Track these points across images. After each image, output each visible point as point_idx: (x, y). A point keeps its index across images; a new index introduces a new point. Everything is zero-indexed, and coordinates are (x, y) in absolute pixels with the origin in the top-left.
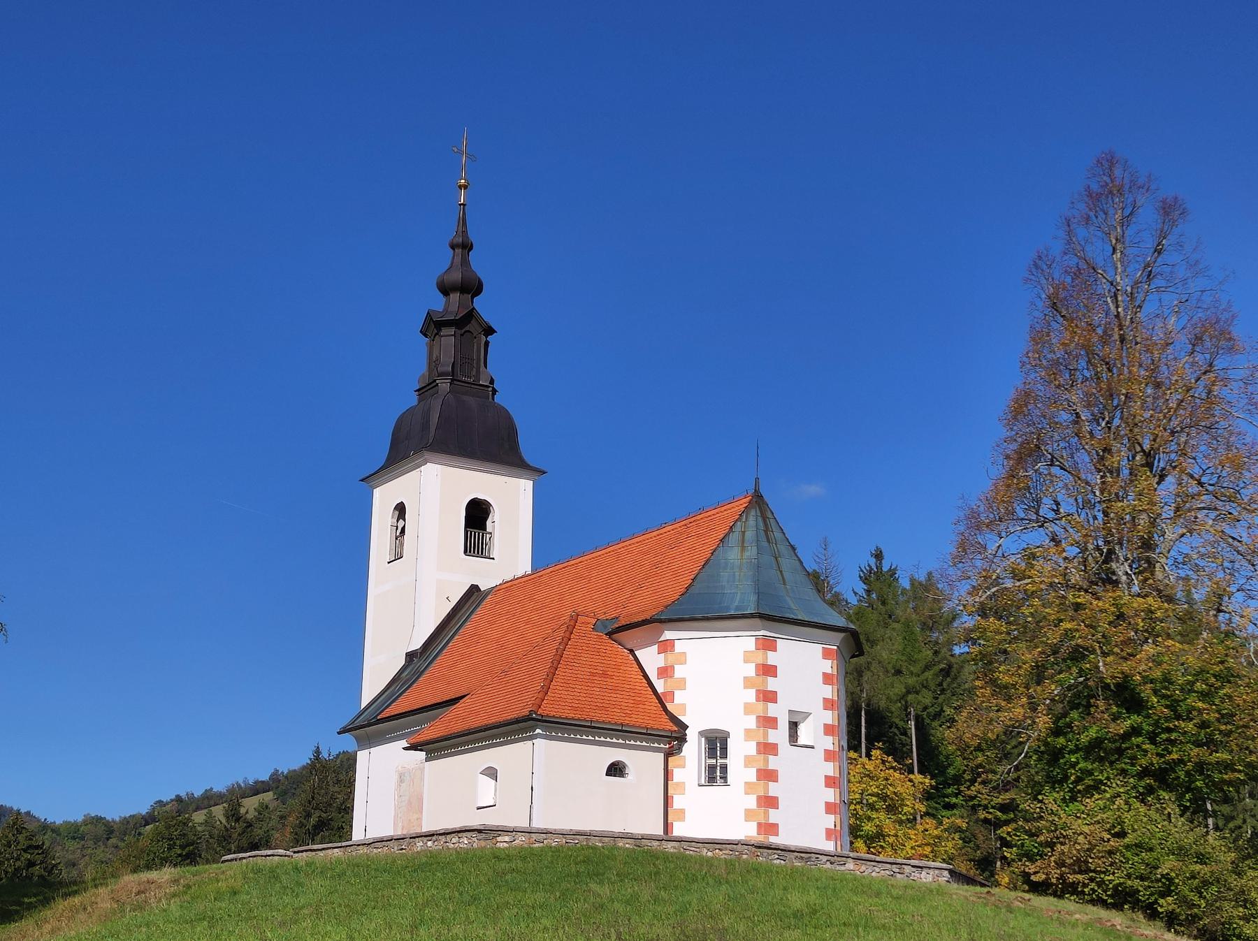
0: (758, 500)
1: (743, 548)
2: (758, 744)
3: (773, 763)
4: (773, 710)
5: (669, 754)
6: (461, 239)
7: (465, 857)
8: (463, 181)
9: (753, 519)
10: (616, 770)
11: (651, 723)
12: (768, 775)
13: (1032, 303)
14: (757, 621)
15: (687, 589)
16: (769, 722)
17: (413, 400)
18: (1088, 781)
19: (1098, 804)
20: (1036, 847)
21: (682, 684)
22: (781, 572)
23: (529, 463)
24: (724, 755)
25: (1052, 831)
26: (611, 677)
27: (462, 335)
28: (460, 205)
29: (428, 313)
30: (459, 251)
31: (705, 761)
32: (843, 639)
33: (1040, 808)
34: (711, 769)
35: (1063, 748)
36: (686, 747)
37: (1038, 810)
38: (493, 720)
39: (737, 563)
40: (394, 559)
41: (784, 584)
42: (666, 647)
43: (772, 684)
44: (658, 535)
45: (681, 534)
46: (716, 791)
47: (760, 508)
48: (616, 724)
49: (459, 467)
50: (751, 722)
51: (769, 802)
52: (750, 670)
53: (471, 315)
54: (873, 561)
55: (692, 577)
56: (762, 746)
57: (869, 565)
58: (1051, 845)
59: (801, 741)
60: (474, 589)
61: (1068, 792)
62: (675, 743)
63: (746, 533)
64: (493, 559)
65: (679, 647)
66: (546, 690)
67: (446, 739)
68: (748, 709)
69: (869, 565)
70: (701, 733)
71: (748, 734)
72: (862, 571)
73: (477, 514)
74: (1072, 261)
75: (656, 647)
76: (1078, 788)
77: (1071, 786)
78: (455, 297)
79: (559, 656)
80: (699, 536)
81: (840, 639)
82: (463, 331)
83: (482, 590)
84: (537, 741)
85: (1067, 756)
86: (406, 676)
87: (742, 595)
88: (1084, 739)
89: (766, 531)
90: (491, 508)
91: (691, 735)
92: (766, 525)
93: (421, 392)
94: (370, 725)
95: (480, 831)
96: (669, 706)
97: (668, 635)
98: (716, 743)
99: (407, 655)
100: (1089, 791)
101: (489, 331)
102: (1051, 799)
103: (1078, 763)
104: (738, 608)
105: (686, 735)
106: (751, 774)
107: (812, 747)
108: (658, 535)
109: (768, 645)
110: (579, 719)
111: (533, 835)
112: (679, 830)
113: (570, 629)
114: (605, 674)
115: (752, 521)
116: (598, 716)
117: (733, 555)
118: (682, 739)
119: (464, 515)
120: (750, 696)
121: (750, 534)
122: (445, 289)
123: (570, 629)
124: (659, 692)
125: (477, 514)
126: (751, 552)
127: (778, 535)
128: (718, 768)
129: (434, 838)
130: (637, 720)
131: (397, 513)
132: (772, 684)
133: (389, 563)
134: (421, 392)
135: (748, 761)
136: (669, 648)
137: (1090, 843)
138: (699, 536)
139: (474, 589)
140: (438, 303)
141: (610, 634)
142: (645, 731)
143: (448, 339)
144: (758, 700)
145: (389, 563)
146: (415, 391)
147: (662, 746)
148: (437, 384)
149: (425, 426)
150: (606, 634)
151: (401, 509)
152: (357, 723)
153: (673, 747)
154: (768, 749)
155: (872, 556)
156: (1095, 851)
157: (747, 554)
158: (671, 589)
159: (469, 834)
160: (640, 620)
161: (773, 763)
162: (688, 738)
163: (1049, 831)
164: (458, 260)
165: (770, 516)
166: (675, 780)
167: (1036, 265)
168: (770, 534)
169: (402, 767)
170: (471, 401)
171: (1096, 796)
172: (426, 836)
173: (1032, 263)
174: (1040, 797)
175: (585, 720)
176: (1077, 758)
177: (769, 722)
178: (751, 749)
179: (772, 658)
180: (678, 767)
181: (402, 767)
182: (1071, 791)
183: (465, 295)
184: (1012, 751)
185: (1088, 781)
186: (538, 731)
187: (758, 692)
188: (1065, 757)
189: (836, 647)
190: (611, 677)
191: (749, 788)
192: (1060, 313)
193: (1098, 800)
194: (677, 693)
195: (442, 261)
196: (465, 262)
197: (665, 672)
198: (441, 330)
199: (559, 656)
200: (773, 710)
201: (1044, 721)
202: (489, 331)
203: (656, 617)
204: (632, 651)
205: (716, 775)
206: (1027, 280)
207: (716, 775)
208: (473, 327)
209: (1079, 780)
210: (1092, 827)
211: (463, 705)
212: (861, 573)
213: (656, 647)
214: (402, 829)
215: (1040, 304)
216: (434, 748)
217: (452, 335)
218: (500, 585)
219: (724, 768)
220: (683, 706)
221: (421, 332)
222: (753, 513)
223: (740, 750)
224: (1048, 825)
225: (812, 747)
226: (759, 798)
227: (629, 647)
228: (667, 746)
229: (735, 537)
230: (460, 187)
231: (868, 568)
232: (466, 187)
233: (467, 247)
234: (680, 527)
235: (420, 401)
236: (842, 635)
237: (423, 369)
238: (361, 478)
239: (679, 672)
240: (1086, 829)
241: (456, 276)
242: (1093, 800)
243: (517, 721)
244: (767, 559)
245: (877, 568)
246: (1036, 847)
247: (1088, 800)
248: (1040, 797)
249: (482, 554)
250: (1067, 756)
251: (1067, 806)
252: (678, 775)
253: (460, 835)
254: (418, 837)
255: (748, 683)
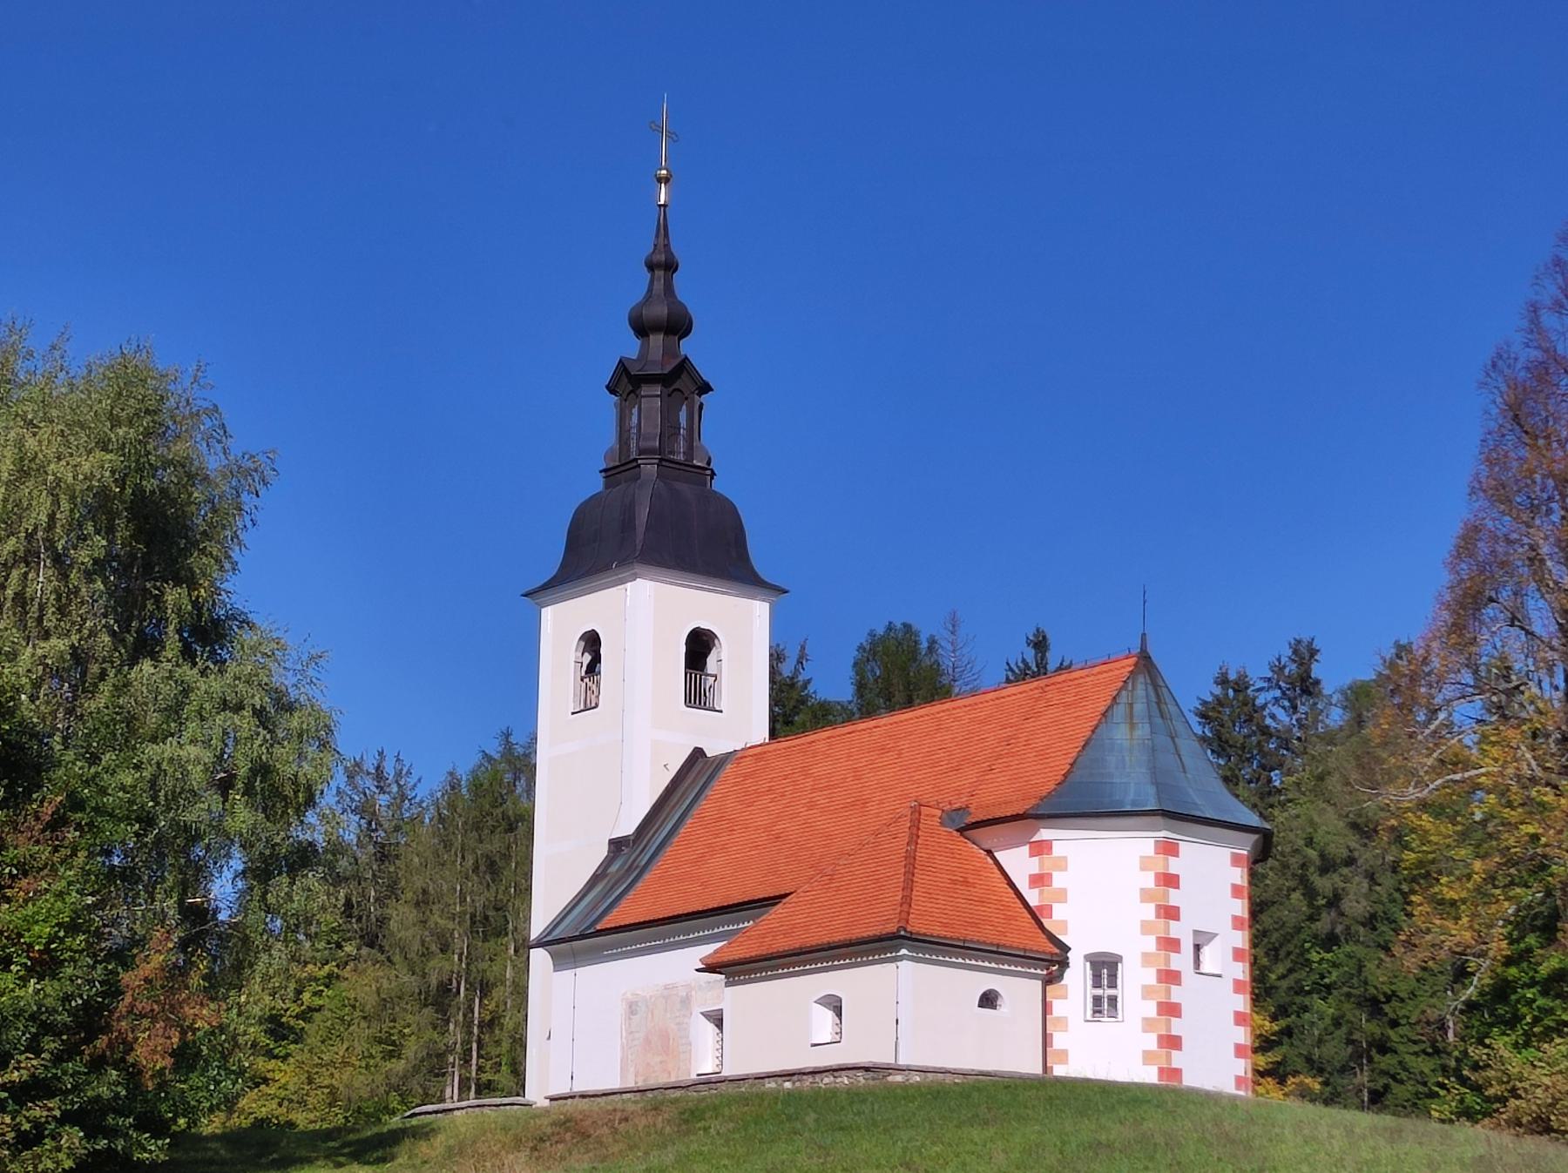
0: (1145, 662)
1: (1132, 726)
2: (1159, 971)
3: (1177, 994)
4: (1176, 929)
5: (1049, 980)
6: (663, 256)
7: (854, 1095)
8: (664, 172)
9: (1141, 688)
10: (988, 1000)
11: (1030, 945)
12: (1170, 1010)
13: (1487, 412)
14: (1159, 820)
15: (1065, 776)
16: (1171, 944)
17: (597, 484)
18: (1548, 1022)
19: (1560, 1051)
20: (1478, 1104)
21: (1062, 896)
22: (1179, 755)
23: (763, 577)
24: (1113, 985)
25: (1503, 1083)
26: (973, 885)
27: (669, 395)
28: (660, 206)
29: (620, 361)
30: (660, 273)
31: (1091, 992)
32: (1257, 841)
33: (1488, 1055)
34: (1097, 1001)
35: (1516, 981)
36: (1068, 974)
37: (1484, 1057)
38: (838, 937)
39: (1126, 744)
40: (582, 707)
41: (1185, 772)
42: (1041, 849)
43: (1174, 897)
44: (997, 699)
45: (1037, 700)
46: (1106, 1026)
47: (1149, 672)
48: (992, 944)
49: (671, 583)
50: (1150, 943)
51: (1172, 1042)
52: (1149, 880)
53: (684, 366)
54: (1030, 654)
55: (1070, 761)
56: (1163, 973)
57: (1024, 661)
58: (1503, 1100)
59: (1205, 968)
60: (698, 753)
61: (1522, 1035)
62: (1054, 968)
63: (1135, 706)
64: (721, 712)
65: (1058, 849)
66: (907, 901)
67: (766, 960)
68: (1146, 928)
69: (1024, 661)
70: (1088, 958)
71: (1147, 959)
72: (1011, 669)
73: (699, 646)
74: (1535, 354)
75: (1026, 848)
76: (1535, 1029)
77: (1526, 1028)
78: (657, 340)
79: (911, 860)
80: (1067, 705)
81: (1251, 843)
82: (671, 389)
83: (708, 755)
84: (904, 964)
85: (1519, 990)
86: (617, 871)
87: (1135, 786)
88: (1544, 970)
89: (1159, 703)
90: (716, 641)
91: (1076, 959)
92: (1158, 696)
93: (609, 473)
94: (582, 937)
95: (867, 1069)
96: (1046, 923)
97: (1045, 834)
98: (1105, 967)
99: (612, 842)
100: (1547, 1035)
101: (705, 388)
102: (1501, 1044)
103: (1534, 1001)
104: (1134, 803)
105: (1068, 958)
106: (1151, 1009)
107: (1219, 976)
108: (997, 699)
109: (1169, 849)
110: (951, 938)
111: (929, 1074)
112: (1059, 1071)
113: (916, 825)
114: (966, 882)
115: (1140, 691)
116: (972, 934)
117: (1120, 733)
118: (1064, 964)
119: (684, 651)
120: (1149, 911)
121: (1139, 707)
122: (641, 328)
123: (916, 825)
124: (1031, 904)
125: (699, 646)
126: (1143, 731)
127: (1172, 708)
128: (1106, 1000)
129: (795, 1078)
130: (1013, 940)
131: (583, 644)
132: (1174, 897)
133: (573, 713)
134: (609, 473)
135: (1147, 992)
136: (1045, 851)
137: (1553, 1098)
138: (1067, 705)
139: (698, 753)
140: (630, 347)
141: (961, 831)
142: (1022, 954)
143: (652, 399)
144: (1158, 916)
145: (573, 713)
146: (601, 472)
147: (1039, 971)
148: (639, 466)
149: (628, 524)
150: (957, 830)
151: (592, 642)
152: (556, 934)
153: (1051, 973)
154: (1170, 977)
155: (1029, 645)
156: (1558, 1106)
157: (1138, 733)
158: (1045, 780)
159: (850, 1073)
160: (1008, 814)
161: (1177, 994)
162: (1071, 961)
163: (1501, 1082)
164: (659, 286)
165: (1161, 684)
166: (1054, 1047)
167: (1494, 365)
168: (1163, 706)
169: (633, 994)
170: (685, 489)
171: (1558, 1040)
172: (784, 1076)
173: (1490, 363)
174: (1487, 1041)
175: (959, 940)
176: (1534, 994)
177: (1171, 944)
178: (1150, 976)
179: (1175, 865)
180: (1056, 998)
181: (633, 994)
182: (1525, 1033)
183: (671, 337)
184: (1278, 984)
185: (1548, 1022)
186: (904, 951)
187: (1158, 907)
188: (1516, 992)
189: (1245, 852)
190: (973, 885)
191: (1148, 1025)
192: (1522, 427)
193: (1559, 1045)
194: (1056, 907)
195: (635, 286)
196: (669, 289)
197: (1039, 880)
198: (639, 387)
199: (911, 860)
200: (1176, 929)
201: (1499, 947)
202: (705, 388)
203: (1031, 812)
204: (990, 853)
205: (1103, 1007)
206: (1484, 384)
207: (1103, 1007)
208: (683, 383)
209: (1536, 1020)
210: (1554, 1078)
211: (773, 916)
212: (1010, 673)
213: (1026, 848)
214: (636, 1076)
215: (1495, 411)
216: (731, 969)
217: (657, 396)
218: (743, 749)
219: (1113, 1000)
220: (1064, 923)
221: (607, 387)
222: (1141, 679)
223: (1135, 979)
224: (1499, 1074)
225: (1219, 976)
226: (1160, 1038)
227: (987, 847)
228: (1045, 972)
229: (1120, 711)
230: (660, 180)
231: (1021, 665)
232: (667, 180)
233: (670, 267)
234: (1031, 690)
235: (607, 486)
236: (1254, 837)
237: (610, 439)
238: (524, 592)
239: (1058, 880)
240: (1546, 1081)
241: (660, 311)
242: (1553, 1044)
243: (879, 939)
244: (1163, 740)
245: (1037, 666)
246: (1478, 1104)
247: (1546, 1046)
248: (1487, 1041)
249: (705, 704)
250: (1519, 990)
251: (1520, 1053)
252: (1059, 1008)
253: (836, 1074)
254: (769, 1077)
255: (1146, 895)
